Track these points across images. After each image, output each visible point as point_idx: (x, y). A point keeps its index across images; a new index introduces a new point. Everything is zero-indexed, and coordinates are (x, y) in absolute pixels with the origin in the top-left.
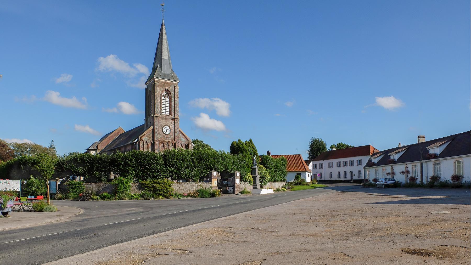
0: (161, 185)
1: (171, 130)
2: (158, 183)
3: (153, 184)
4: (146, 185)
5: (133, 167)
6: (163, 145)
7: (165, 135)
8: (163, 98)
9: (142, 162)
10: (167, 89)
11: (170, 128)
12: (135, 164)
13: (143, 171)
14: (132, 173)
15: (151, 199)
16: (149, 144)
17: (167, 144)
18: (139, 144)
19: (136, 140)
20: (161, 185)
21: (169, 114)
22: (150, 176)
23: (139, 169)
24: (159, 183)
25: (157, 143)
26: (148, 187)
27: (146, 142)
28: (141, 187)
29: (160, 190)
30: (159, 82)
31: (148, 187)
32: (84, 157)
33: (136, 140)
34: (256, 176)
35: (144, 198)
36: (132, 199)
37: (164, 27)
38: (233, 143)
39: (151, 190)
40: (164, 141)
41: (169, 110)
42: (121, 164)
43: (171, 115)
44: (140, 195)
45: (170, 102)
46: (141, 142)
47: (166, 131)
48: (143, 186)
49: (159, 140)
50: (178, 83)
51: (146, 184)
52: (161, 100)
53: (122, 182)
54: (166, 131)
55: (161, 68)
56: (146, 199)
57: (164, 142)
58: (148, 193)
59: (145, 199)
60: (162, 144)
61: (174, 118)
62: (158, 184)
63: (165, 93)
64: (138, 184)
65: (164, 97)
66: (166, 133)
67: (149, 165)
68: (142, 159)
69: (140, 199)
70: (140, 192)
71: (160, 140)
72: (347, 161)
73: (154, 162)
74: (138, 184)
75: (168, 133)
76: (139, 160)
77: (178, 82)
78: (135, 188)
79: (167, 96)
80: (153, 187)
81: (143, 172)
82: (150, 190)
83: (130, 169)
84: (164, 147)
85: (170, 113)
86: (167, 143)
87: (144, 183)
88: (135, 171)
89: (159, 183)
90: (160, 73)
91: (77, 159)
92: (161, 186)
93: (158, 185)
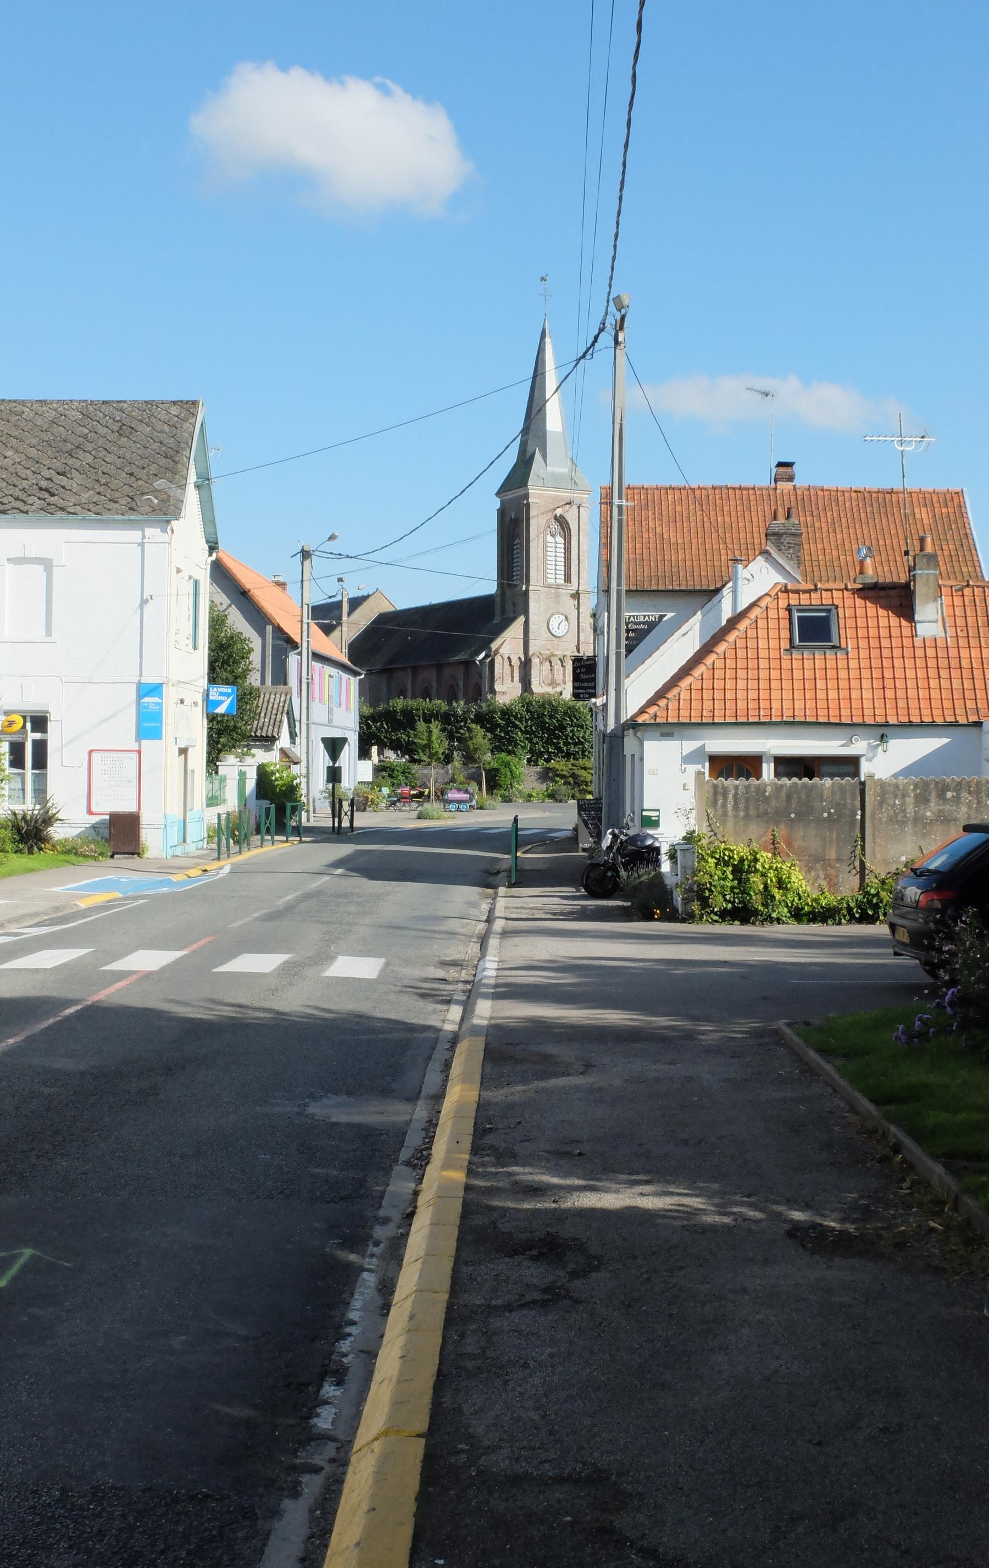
0: (589, 773)
1: (569, 624)
2: (582, 768)
3: (571, 769)
4: (558, 772)
5: (526, 732)
6: (551, 666)
7: (553, 638)
8: (549, 538)
9: (547, 723)
10: (561, 515)
11: (566, 618)
12: (531, 726)
13: (549, 742)
14: (523, 745)
15: (569, 802)
16: (516, 663)
17: (559, 662)
18: (492, 664)
19: (483, 655)
20: (589, 773)
21: (565, 582)
22: (563, 751)
23: (538, 737)
24: (585, 769)
25: (535, 661)
26: (562, 777)
27: (509, 658)
28: (546, 776)
29: (587, 782)
30: (539, 496)
31: (562, 777)
32: (412, 708)
33: (483, 655)
34: (409, 693)
35: (555, 799)
36: (529, 801)
37: (548, 340)
38: (380, 1315)
39: (570, 784)
40: (553, 655)
41: (565, 571)
42: (499, 725)
43: (569, 585)
44: (546, 793)
45: (568, 549)
46: (498, 660)
47: (559, 629)
48: (550, 775)
49: (540, 653)
50: (587, 496)
51: (557, 770)
52: (545, 541)
53: (507, 765)
54: (559, 629)
55: (544, 457)
56: (561, 801)
57: (552, 659)
58: (564, 788)
59: (556, 800)
60: (547, 664)
61: (578, 593)
62: (583, 771)
63: (555, 526)
64: (538, 769)
65: (551, 535)
66: (557, 634)
67: (562, 728)
68: (546, 715)
69: (546, 800)
70: (544, 786)
71: (542, 652)
72: (33, 774)
73: (572, 721)
74: (538, 770)
75: (561, 634)
76: (539, 717)
77: (588, 494)
78: (533, 778)
79: (560, 533)
80: (574, 776)
81: (547, 743)
82: (566, 783)
83: (519, 736)
84: (551, 670)
85: (568, 578)
86: (560, 659)
87: (554, 768)
88: (530, 740)
89: (585, 769)
90: (542, 474)
91: (395, 711)
92: (590, 775)
93: (583, 773)
